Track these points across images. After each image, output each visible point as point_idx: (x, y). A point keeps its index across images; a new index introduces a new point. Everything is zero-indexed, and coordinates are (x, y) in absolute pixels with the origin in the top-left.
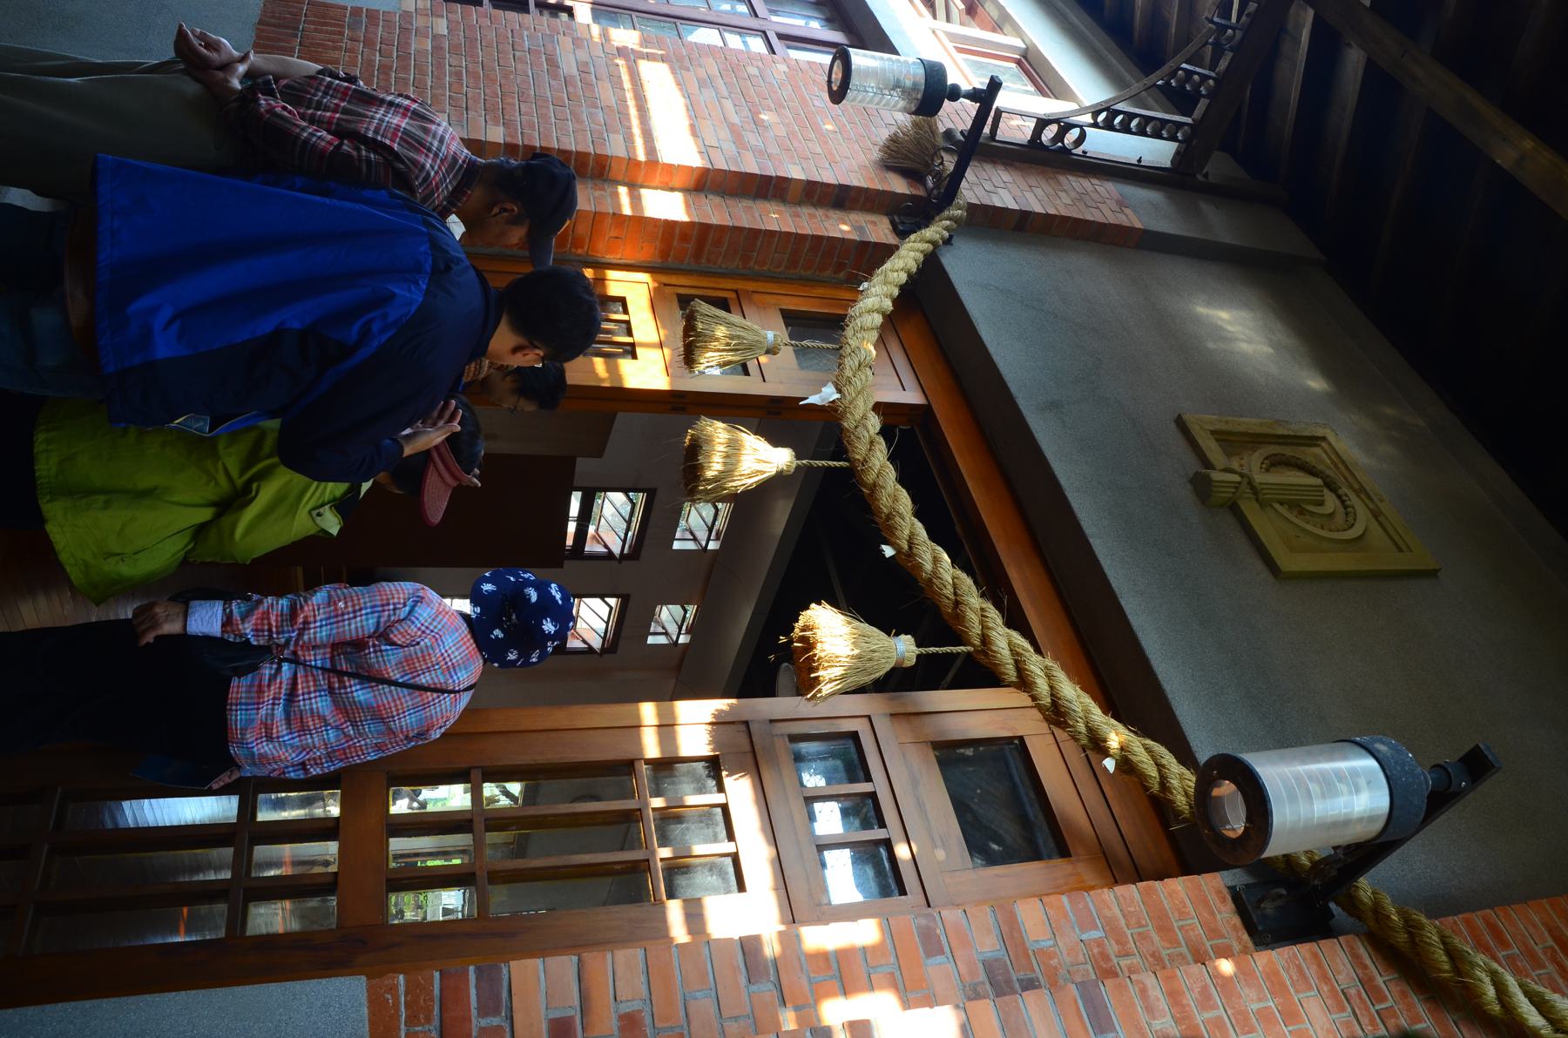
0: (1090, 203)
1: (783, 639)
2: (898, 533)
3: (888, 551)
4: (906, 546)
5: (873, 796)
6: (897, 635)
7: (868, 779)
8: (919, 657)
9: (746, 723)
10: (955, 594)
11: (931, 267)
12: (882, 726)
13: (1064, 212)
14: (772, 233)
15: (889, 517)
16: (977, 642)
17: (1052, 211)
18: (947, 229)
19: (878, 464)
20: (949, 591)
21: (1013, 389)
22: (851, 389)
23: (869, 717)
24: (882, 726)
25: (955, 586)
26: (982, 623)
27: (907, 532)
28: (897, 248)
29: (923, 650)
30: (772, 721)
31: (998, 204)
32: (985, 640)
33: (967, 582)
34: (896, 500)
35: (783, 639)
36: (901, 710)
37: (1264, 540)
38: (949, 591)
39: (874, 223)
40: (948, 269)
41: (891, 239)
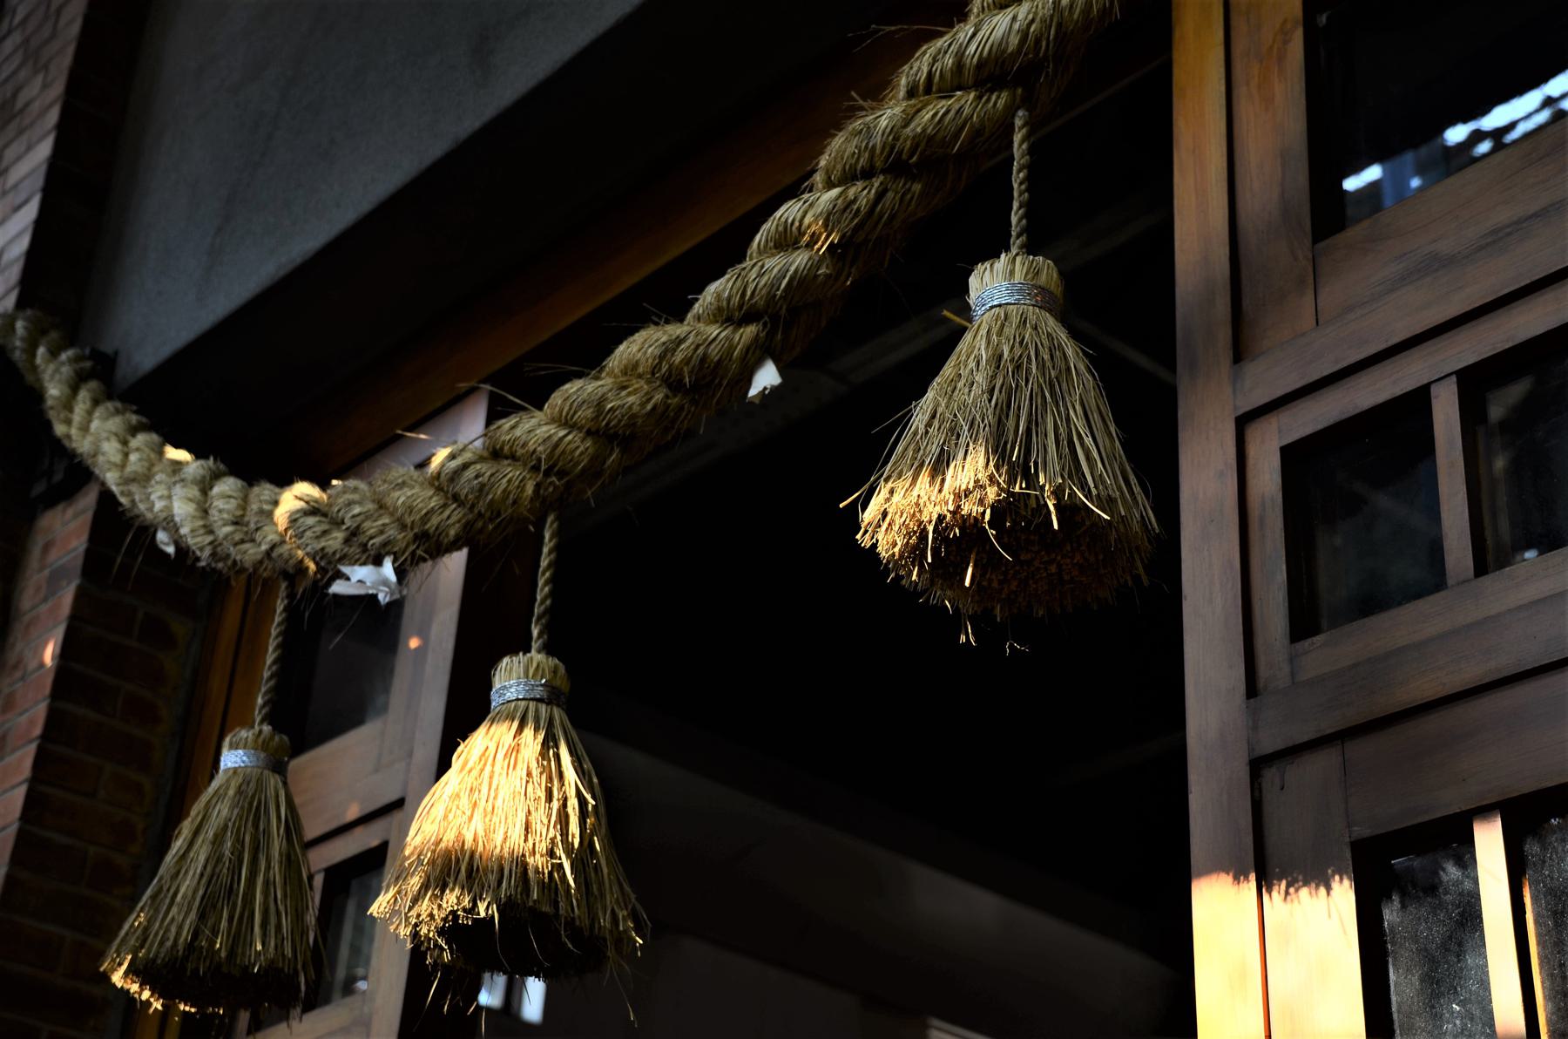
0: (46, 31)
1: (967, 637)
2: (714, 352)
3: (767, 377)
4: (750, 331)
5: (1475, 383)
6: (965, 310)
7: (1418, 402)
8: (1030, 249)
9: (1258, 765)
10: (867, 174)
11: (169, 403)
12: (1268, 378)
13: (58, 89)
14: (32, 802)
15: (673, 382)
16: (1000, 100)
17: (53, 116)
18: (54, 354)
19: (543, 431)
20: (863, 194)
21: (436, 150)
22: (371, 527)
23: (1243, 422)
24: (1268, 378)
25: (848, 178)
26: (946, 92)
27: (714, 331)
28: (107, 497)
29: (1016, 244)
30: (1252, 690)
31: (24, 243)
32: (991, 73)
33: (840, 147)
34: (631, 369)
35: (967, 637)
36: (1224, 334)
37: (1506, 291)
38: (863, 194)
39: (46, 548)
40: (166, 351)
41: (88, 500)
